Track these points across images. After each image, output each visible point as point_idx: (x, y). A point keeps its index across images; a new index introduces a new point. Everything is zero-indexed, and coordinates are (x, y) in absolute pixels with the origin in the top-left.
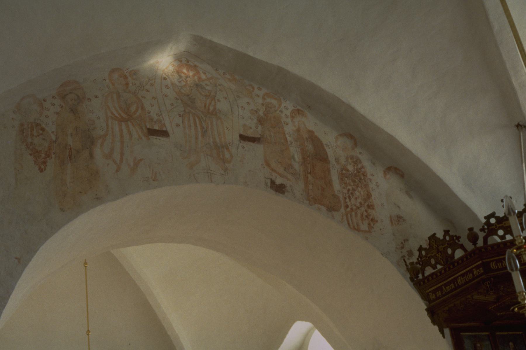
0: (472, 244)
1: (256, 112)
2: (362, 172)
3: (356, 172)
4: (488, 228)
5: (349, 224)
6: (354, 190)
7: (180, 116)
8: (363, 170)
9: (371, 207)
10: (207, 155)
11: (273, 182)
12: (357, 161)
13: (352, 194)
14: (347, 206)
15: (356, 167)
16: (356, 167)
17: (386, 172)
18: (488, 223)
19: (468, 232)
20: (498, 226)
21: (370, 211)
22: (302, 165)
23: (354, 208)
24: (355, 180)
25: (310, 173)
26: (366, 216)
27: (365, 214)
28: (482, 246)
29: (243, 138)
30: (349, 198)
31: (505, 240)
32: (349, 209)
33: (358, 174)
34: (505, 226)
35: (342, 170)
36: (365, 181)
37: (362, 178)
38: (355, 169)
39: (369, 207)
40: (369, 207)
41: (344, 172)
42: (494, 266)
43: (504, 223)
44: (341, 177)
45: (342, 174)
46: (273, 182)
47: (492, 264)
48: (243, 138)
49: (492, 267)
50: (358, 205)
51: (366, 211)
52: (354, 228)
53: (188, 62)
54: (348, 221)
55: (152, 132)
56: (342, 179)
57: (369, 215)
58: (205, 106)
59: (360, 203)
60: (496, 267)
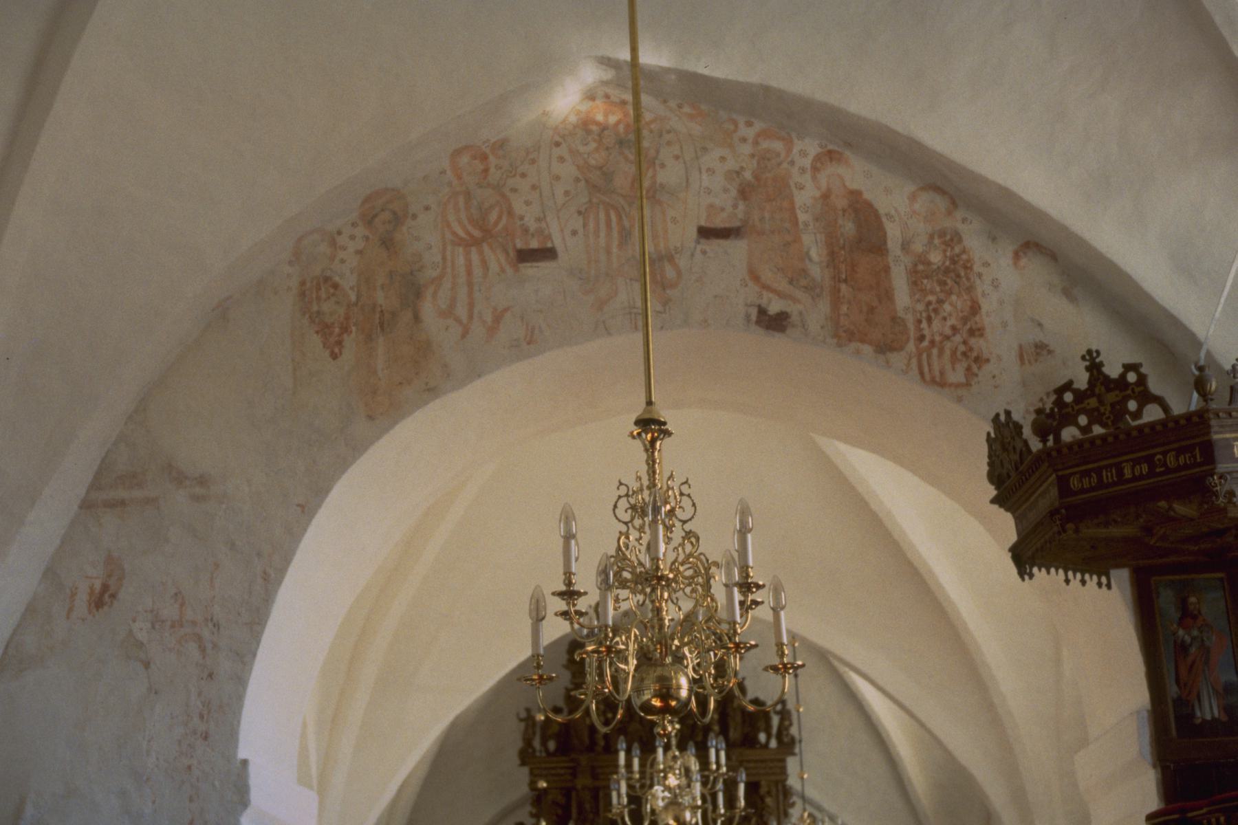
3: (948, 263)
6: (940, 302)
7: (580, 213)
8: (964, 257)
9: (977, 333)
11: (762, 311)
13: (935, 311)
14: (922, 338)
15: (948, 254)
16: (948, 254)
17: (1021, 254)
18: (1059, 402)
20: (1076, 408)
21: (973, 341)
23: (937, 338)
24: (945, 281)
25: (845, 281)
26: (964, 354)
27: (962, 348)
30: (929, 319)
31: (1091, 435)
32: (925, 343)
33: (952, 266)
34: (1088, 407)
36: (968, 279)
37: (963, 274)
40: (972, 332)
41: (921, 267)
42: (1076, 483)
46: (762, 311)
47: (1074, 479)
49: (1072, 486)
50: (948, 331)
51: (965, 343)
57: (971, 349)
59: (954, 328)
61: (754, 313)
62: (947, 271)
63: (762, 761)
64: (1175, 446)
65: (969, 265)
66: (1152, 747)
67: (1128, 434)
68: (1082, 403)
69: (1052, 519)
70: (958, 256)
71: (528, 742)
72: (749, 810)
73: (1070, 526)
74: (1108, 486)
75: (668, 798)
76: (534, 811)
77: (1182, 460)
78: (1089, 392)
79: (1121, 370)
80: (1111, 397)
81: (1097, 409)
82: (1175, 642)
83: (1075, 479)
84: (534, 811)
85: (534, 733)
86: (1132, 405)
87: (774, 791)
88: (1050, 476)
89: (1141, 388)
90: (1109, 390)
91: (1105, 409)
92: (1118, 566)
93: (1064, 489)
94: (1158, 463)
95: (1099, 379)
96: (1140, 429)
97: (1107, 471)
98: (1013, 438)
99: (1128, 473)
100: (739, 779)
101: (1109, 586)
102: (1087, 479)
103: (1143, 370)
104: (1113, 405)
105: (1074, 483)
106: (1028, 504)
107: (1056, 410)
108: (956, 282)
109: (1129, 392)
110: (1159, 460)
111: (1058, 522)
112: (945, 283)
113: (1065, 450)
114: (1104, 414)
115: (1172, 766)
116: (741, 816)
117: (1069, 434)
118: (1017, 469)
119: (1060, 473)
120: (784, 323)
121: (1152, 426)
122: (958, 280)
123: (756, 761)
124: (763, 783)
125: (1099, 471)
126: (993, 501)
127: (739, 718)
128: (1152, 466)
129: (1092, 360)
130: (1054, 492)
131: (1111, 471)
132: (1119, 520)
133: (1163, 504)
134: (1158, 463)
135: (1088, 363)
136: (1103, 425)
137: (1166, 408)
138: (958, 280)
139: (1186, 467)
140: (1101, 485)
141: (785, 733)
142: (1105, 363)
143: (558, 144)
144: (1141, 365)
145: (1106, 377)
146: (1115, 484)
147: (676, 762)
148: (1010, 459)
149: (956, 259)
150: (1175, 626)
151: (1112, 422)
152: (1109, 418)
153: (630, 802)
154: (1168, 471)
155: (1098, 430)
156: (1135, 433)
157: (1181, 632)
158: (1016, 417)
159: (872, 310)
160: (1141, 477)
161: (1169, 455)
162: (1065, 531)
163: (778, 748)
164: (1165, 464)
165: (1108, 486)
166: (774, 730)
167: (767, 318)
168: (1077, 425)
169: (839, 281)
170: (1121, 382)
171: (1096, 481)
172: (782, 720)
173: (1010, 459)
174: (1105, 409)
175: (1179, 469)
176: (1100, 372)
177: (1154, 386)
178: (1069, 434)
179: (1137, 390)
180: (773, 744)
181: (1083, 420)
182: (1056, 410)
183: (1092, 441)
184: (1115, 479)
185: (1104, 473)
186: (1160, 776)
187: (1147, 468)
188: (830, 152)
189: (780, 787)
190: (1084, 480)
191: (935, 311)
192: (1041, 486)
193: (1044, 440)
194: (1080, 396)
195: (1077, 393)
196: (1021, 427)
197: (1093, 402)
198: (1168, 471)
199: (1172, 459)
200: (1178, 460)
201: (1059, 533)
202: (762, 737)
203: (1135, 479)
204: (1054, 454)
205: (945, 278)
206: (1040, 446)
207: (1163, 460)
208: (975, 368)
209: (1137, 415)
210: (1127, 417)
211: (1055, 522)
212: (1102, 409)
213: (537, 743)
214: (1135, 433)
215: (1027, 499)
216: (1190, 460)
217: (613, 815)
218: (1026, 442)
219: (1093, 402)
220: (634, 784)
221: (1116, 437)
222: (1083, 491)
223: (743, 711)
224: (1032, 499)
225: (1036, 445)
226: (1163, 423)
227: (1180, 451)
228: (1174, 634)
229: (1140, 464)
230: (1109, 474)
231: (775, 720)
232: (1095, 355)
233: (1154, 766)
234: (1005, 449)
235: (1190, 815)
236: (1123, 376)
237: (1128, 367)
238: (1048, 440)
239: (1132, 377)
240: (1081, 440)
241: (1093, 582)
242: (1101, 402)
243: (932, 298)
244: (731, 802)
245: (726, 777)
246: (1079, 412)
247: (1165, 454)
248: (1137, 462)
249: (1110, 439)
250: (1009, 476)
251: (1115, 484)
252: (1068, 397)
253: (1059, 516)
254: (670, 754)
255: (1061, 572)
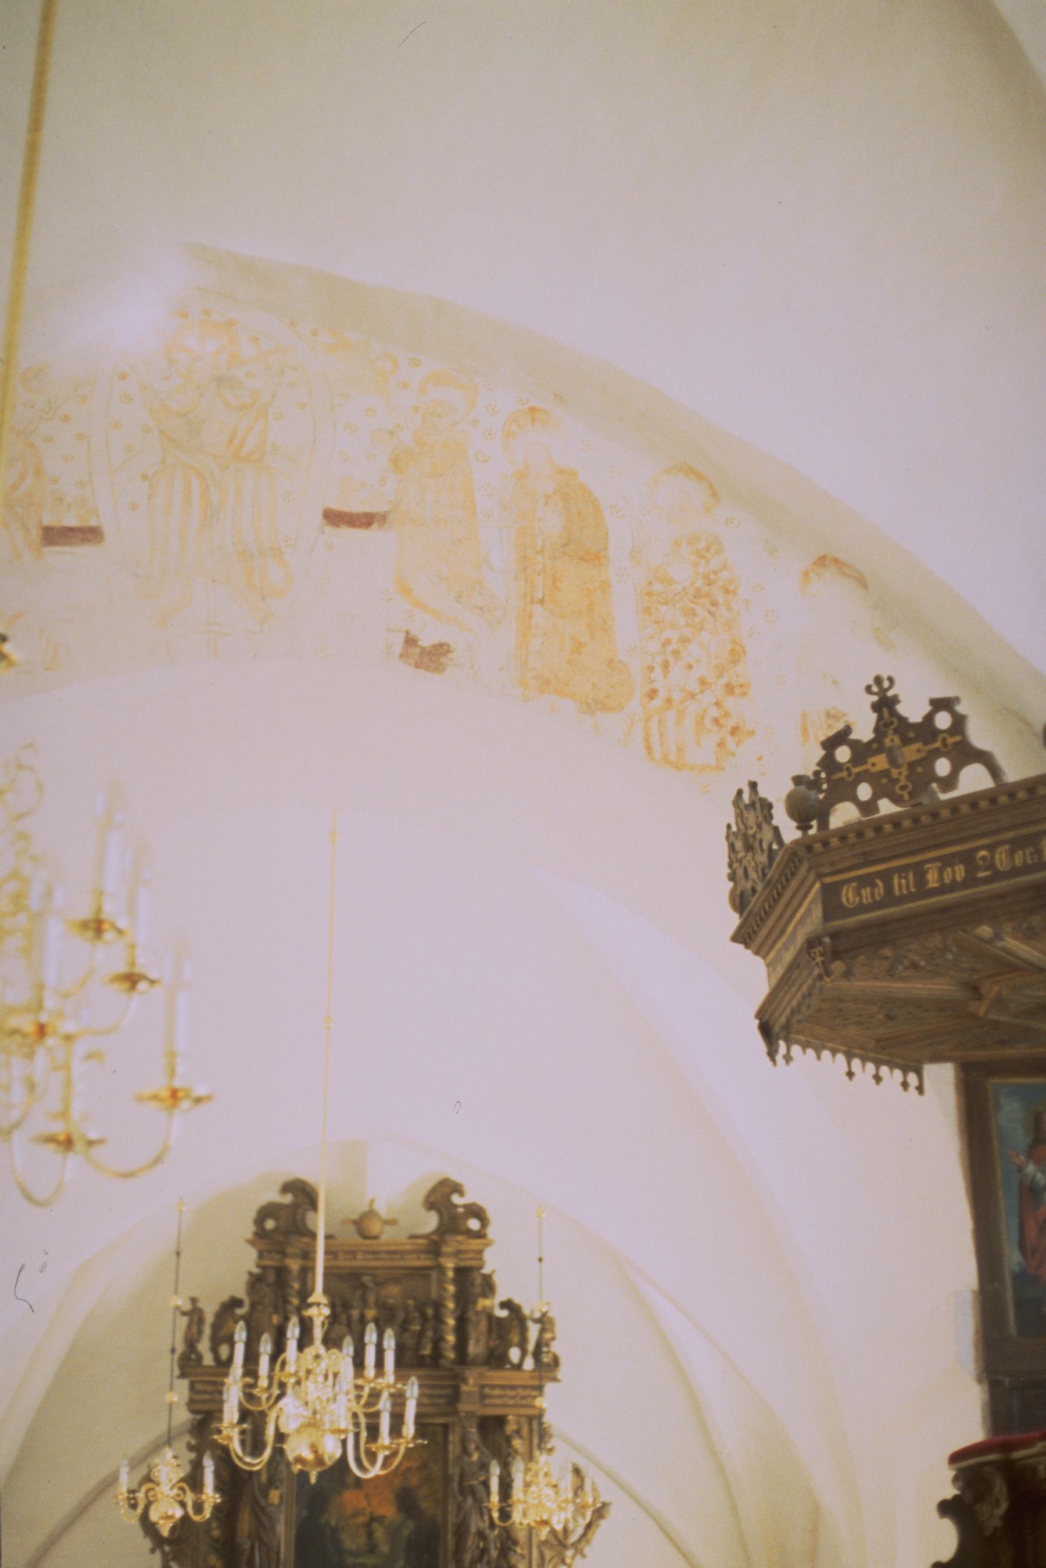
0: (795, 824)
1: (391, 433)
2: (721, 583)
3: (699, 583)
4: (828, 780)
5: (649, 748)
6: (685, 640)
7: (145, 477)
8: (725, 575)
9: (738, 690)
10: (214, 581)
11: (410, 641)
12: (708, 549)
13: (676, 653)
14: (652, 694)
15: (701, 570)
16: (701, 570)
17: (812, 575)
18: (828, 763)
19: (791, 786)
20: (855, 770)
21: (729, 702)
22: (516, 578)
23: (677, 696)
24: (693, 610)
25: (542, 601)
26: (716, 721)
27: (714, 712)
28: (799, 839)
29: (334, 518)
30: (666, 665)
31: (877, 816)
32: (658, 702)
33: (707, 588)
34: (874, 770)
35: (650, 583)
36: (729, 609)
37: (721, 601)
38: (698, 574)
39: (730, 689)
40: (730, 689)
41: (657, 587)
42: (851, 896)
43: (922, 755)
44: (646, 604)
45: (649, 594)
46: (410, 641)
47: (847, 891)
48: (334, 518)
49: (844, 900)
50: (694, 686)
51: (718, 704)
52: (666, 759)
53: (207, 313)
54: (647, 739)
55: (54, 536)
56: (647, 610)
57: (727, 715)
58: (231, 441)
59: (702, 682)
60: (854, 901)
61: (398, 643)
62: (698, 595)
63: (513, 1387)
64: (1010, 835)
65: (731, 588)
66: (977, 1350)
67: (935, 815)
68: (864, 763)
69: (809, 954)
70: (715, 573)
71: (191, 1343)
72: (420, 1441)
73: (838, 967)
74: (902, 899)
75: (304, 1417)
76: (193, 1442)
77: (1019, 859)
78: (875, 746)
79: (928, 708)
80: (912, 752)
81: (886, 773)
82: (1021, 1182)
83: (850, 889)
84: (193, 1442)
85: (200, 1332)
86: (943, 767)
87: (525, 1430)
88: (812, 885)
89: (958, 738)
90: (906, 741)
91: (900, 774)
92: (936, 1058)
93: (832, 907)
94: (981, 863)
95: (892, 723)
96: (954, 805)
97: (900, 878)
98: (759, 826)
99: (932, 879)
100: (408, 1394)
101: (920, 1089)
102: (868, 889)
103: (960, 709)
104: (912, 765)
105: (848, 896)
106: (783, 939)
107: (823, 775)
108: (710, 613)
109: (938, 744)
110: (983, 858)
111: (819, 959)
112: (694, 613)
113: (835, 842)
114: (897, 780)
115: (1007, 1381)
116: (408, 1449)
117: (843, 815)
118: (764, 875)
119: (828, 880)
120: (442, 660)
121: (973, 800)
122: (713, 609)
123: (502, 1387)
124: (510, 1417)
125: (886, 876)
126: (735, 938)
127: (483, 1326)
128: (971, 865)
129: (883, 691)
130: (817, 913)
131: (906, 878)
132: (922, 963)
133: (985, 931)
134: (981, 863)
135: (875, 698)
136: (896, 800)
137: (995, 771)
138: (713, 609)
139: (1026, 869)
140: (889, 899)
141: (545, 1349)
142: (901, 698)
143: (123, 377)
144: (957, 700)
145: (903, 720)
146: (910, 898)
147: (318, 1365)
148: (756, 863)
149: (712, 577)
150: (1022, 1158)
151: (910, 794)
152: (903, 788)
153: (242, 1419)
154: (998, 876)
155: (886, 807)
156: (945, 813)
157: (1031, 1168)
158: (763, 792)
159: (578, 647)
160: (954, 886)
161: (998, 851)
162: (828, 973)
163: (534, 1370)
164: (991, 866)
165: (902, 899)
166: (531, 1346)
167: (418, 650)
168: (855, 799)
169: (532, 602)
170: (926, 729)
171: (882, 892)
172: (542, 1331)
173: (756, 863)
174: (900, 774)
175: (1015, 872)
176: (893, 713)
177: (978, 736)
178: (843, 815)
179: (951, 740)
180: (529, 1364)
181: (864, 791)
182: (823, 775)
183: (878, 827)
184: (913, 890)
185: (896, 881)
186: (987, 1397)
187: (963, 872)
188: (533, 410)
189: (535, 1426)
190: (863, 891)
191: (676, 653)
192: (800, 905)
193: (804, 827)
194: (861, 752)
195: (856, 747)
196: (770, 806)
197: (880, 762)
198: (998, 876)
199: (1003, 856)
200: (1012, 858)
201: (820, 977)
202: (514, 1354)
203: (943, 889)
204: (818, 846)
205: (693, 606)
206: (798, 834)
207: (989, 857)
208: (731, 742)
209: (949, 782)
210: (934, 785)
211: (814, 959)
212: (895, 772)
213: (204, 1346)
214: (945, 813)
215: (782, 932)
216: (1032, 859)
217: (223, 1439)
218: (776, 830)
219: (880, 762)
220: (259, 1395)
221: (916, 820)
222: (861, 908)
223: (490, 1316)
224: (790, 929)
225: (790, 832)
226: (989, 796)
227: (1016, 844)
228: (1020, 1169)
229: (952, 865)
230: (903, 881)
231: (533, 1331)
232: (886, 684)
233: (980, 1381)
234: (749, 848)
235: (1018, 1454)
236: (929, 718)
237: (940, 704)
238: (811, 827)
239: (943, 721)
240: (860, 823)
241: (892, 1077)
242: (893, 761)
243: (672, 635)
244: (396, 1430)
245: (392, 1390)
246: (859, 779)
247: (992, 848)
248: (947, 862)
249: (907, 823)
250: (754, 890)
251: (910, 898)
252: (843, 754)
253: (820, 948)
254: (310, 1352)
255: (841, 1058)
